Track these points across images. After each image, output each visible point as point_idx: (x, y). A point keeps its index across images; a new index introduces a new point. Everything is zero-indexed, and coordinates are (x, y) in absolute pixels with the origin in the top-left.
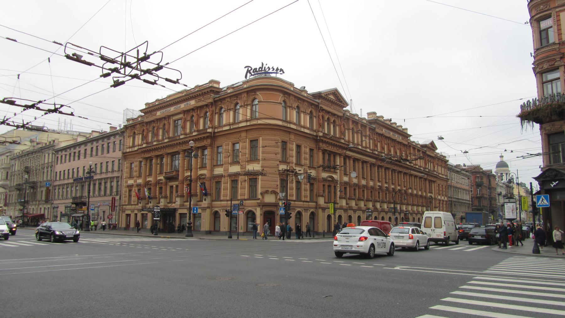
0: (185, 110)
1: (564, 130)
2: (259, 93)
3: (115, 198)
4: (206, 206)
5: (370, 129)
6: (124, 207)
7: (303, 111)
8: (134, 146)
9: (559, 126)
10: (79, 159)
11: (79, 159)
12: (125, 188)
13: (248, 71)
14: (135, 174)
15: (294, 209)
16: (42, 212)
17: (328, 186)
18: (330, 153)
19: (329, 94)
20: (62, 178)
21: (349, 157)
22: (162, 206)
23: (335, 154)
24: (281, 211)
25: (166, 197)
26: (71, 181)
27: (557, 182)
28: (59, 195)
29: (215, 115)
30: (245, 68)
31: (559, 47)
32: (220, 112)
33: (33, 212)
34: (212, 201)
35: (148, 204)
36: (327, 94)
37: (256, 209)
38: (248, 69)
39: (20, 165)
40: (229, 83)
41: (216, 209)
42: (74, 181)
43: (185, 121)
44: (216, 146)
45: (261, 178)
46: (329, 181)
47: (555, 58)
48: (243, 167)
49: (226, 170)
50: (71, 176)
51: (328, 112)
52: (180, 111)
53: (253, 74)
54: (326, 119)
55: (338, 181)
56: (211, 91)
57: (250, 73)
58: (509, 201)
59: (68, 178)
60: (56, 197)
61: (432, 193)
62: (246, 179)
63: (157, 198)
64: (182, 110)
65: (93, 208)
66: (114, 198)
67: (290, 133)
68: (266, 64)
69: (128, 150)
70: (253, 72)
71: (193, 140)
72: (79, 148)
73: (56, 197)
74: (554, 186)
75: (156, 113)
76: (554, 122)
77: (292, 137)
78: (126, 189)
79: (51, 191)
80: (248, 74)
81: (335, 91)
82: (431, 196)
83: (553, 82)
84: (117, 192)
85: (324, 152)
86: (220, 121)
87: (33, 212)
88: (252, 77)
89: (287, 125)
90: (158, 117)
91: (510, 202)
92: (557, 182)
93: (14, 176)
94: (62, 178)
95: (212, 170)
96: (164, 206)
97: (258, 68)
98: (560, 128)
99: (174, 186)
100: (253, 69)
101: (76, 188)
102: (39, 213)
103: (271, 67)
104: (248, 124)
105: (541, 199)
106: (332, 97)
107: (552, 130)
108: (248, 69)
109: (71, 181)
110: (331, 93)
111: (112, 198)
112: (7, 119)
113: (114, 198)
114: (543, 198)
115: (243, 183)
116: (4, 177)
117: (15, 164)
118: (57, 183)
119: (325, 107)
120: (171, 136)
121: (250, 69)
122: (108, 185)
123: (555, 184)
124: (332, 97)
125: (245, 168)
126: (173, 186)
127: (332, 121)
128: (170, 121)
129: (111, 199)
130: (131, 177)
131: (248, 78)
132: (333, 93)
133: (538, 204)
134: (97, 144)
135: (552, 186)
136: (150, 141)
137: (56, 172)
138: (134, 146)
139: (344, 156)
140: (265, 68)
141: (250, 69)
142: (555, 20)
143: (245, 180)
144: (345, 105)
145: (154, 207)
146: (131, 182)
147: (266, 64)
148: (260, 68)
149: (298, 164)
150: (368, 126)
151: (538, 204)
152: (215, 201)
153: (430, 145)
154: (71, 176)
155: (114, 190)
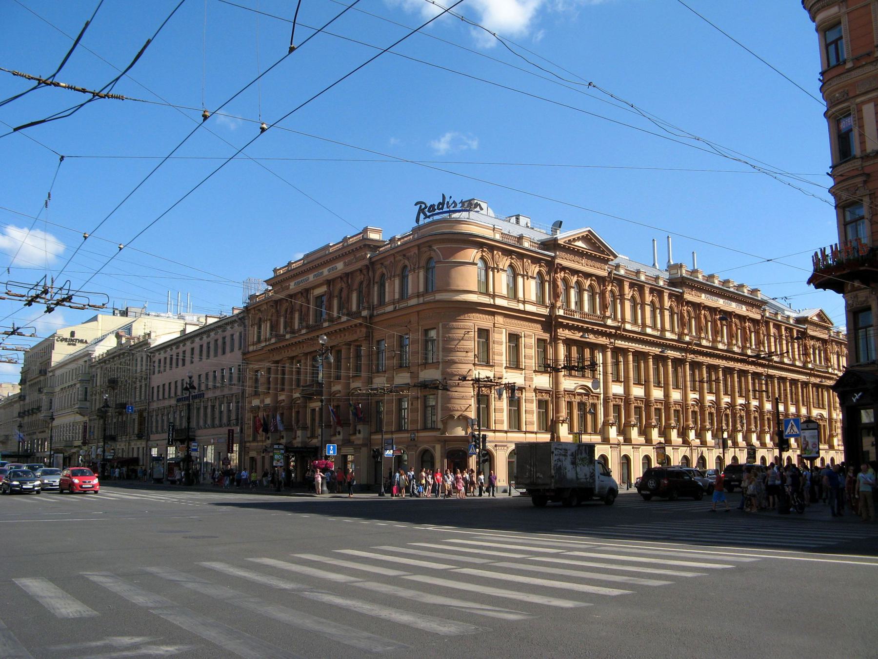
0: (330, 279)
1: (870, 305)
2: (437, 248)
3: (233, 430)
4: (360, 442)
5: (671, 296)
6: (248, 444)
7: (522, 273)
8: (259, 341)
9: (864, 299)
10: (184, 365)
11: (184, 365)
12: (248, 412)
13: (421, 210)
14: (261, 389)
15: (506, 446)
16: (135, 455)
17: (578, 403)
18: (581, 345)
19: (574, 239)
20: (161, 397)
21: (624, 351)
22: (299, 442)
23: (593, 347)
24: (471, 449)
25: (305, 428)
26: (173, 402)
27: (860, 394)
28: (157, 427)
29: (374, 287)
30: (416, 205)
31: (862, 165)
32: (402, 273)
33: (123, 455)
34: (371, 433)
35: (355, 434)
36: (569, 240)
37: (434, 447)
38: (421, 206)
39: (102, 376)
40: (93, 338)
41: (426, 446)
42: (177, 401)
43: (330, 298)
44: (375, 341)
45: (442, 394)
46: (580, 394)
47: (855, 183)
48: (414, 375)
49: (390, 380)
50: (173, 394)
51: (574, 272)
52: (322, 282)
53: (428, 214)
54: (573, 284)
55: (600, 394)
56: (365, 245)
57: (425, 214)
58: (807, 426)
59: (170, 397)
60: (154, 429)
61: (823, 408)
62: (419, 396)
63: (331, 426)
64: (324, 279)
65: (196, 448)
66: (231, 431)
67: (493, 314)
68: (451, 197)
69: (251, 348)
70: (429, 211)
71: (325, 334)
72: (183, 346)
73: (154, 429)
74: (857, 400)
75: (289, 285)
76: (857, 292)
77: (499, 319)
78: (250, 414)
79: (147, 418)
80: (422, 216)
81: (587, 233)
82: (821, 415)
83: (858, 222)
84: (237, 419)
85: (569, 343)
86: (382, 294)
87: (123, 455)
88: (427, 220)
89: (488, 300)
90: (292, 292)
91: (810, 428)
92: (860, 394)
93: (95, 395)
94: (161, 397)
95: (370, 381)
96: (302, 442)
97: (436, 204)
98: (864, 301)
99: (317, 409)
100: (428, 205)
101: (181, 413)
102: (131, 456)
103: (458, 202)
104: (421, 300)
105: (790, 425)
106: (580, 244)
107: (855, 305)
108: (421, 206)
109: (173, 402)
110: (578, 238)
111: (229, 430)
112: (18, 328)
113: (231, 431)
114: (793, 424)
115: (415, 403)
116: (81, 397)
117: (97, 375)
118: (154, 406)
119: (565, 263)
120: (311, 323)
121: (423, 206)
122: (224, 408)
123: (857, 397)
124: (580, 244)
125: (418, 377)
126: (315, 409)
127: (587, 288)
128: (309, 297)
129: (227, 432)
130: (256, 394)
131: (421, 222)
132: (583, 236)
133: (786, 433)
134: (177, 351)
135: (854, 400)
136: (296, 327)
137: (153, 388)
138: (259, 341)
139: (611, 348)
140: (448, 202)
141: (423, 206)
142: (855, 117)
143: (418, 398)
144: (610, 256)
145: (272, 445)
146: (256, 402)
147: (451, 197)
148: (440, 203)
149: (515, 364)
150: (665, 291)
151: (786, 433)
152: (376, 432)
153: (815, 318)
154: (173, 394)
155: (233, 417)
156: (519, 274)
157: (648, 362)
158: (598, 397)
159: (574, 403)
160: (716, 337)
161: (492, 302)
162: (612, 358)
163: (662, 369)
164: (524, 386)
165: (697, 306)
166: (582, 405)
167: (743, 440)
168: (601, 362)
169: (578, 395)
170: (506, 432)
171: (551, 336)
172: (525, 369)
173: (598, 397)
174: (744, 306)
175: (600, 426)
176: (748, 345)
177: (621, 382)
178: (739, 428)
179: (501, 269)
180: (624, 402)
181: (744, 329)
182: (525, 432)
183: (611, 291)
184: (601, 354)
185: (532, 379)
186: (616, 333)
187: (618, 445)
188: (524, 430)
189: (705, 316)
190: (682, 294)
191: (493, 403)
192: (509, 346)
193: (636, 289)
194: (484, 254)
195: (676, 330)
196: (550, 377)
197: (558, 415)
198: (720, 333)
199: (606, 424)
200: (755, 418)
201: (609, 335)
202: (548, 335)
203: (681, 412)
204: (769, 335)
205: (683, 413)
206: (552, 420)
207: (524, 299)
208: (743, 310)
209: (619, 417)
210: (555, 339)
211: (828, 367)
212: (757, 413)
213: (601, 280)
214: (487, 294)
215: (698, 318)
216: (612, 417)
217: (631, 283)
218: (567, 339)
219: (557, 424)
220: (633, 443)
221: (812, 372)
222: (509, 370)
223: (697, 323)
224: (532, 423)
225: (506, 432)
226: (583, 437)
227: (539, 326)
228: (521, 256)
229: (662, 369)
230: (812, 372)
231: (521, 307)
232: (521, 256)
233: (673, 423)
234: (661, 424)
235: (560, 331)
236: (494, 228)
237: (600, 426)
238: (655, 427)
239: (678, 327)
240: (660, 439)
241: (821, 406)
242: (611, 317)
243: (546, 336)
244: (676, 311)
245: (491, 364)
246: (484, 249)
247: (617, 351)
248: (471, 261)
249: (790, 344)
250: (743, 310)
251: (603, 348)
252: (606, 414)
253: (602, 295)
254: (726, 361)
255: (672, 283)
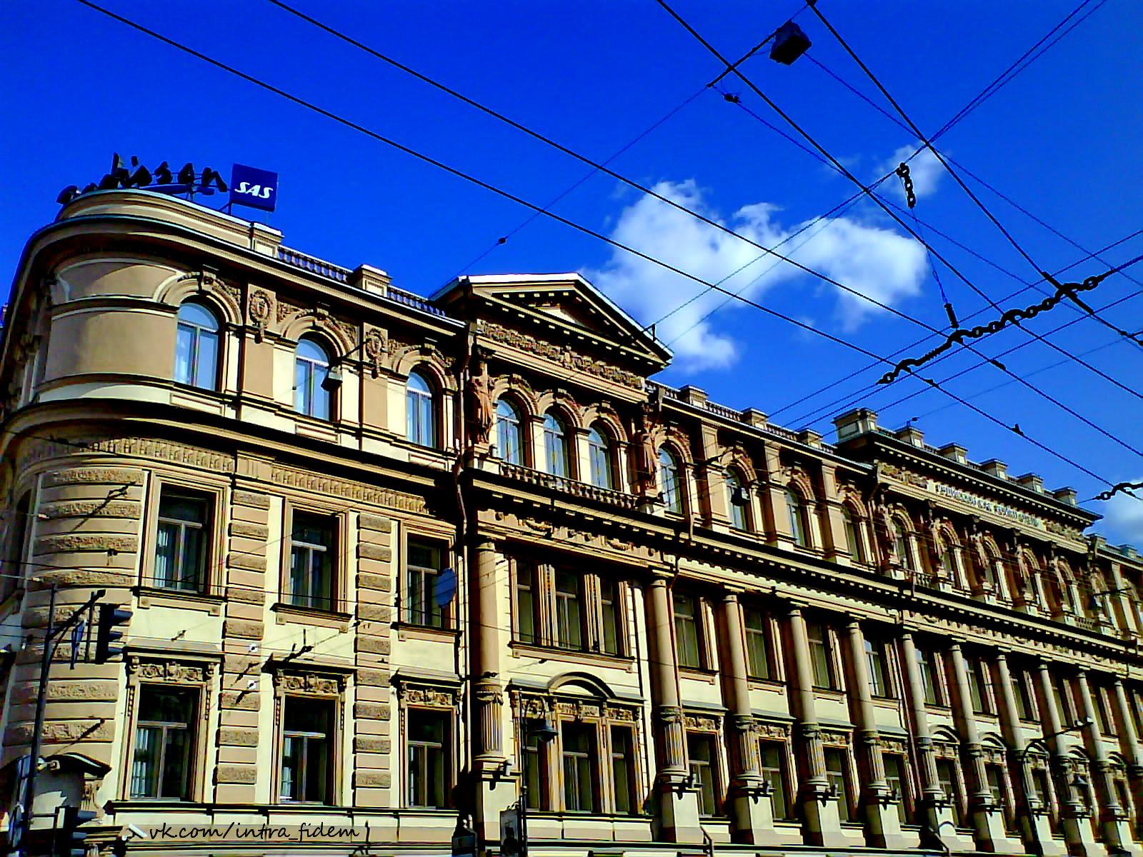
5: (842, 476)
61: (619, 654)
82: (600, 693)
150: (824, 461)
156: (445, 391)
157: (952, 657)
158: (634, 709)
159: (599, 730)
160: (980, 582)
161: (230, 414)
162: (1012, 675)
163: (1030, 682)
164: (350, 664)
165: (918, 508)
166: (579, 735)
167: (1098, 841)
168: (990, 682)
169: (560, 700)
170: (264, 811)
171: (459, 530)
172: (225, 599)
173: (634, 709)
174: (1039, 520)
175: (644, 793)
176: (1066, 607)
177: (713, 673)
178: (1119, 811)
179: (384, 370)
180: (793, 735)
181: (1048, 574)
182: (210, 809)
183: (667, 446)
184: (638, 592)
185: (383, 649)
186: (677, 538)
187: (704, 848)
188: (348, 803)
189: (942, 533)
190: (873, 472)
191: (214, 713)
192: (747, 633)
193: (851, 486)
194: (795, 477)
195: (449, 442)
196: (457, 645)
197: (667, 771)
198: (1028, 583)
199: (663, 787)
200: (1118, 784)
201: (657, 543)
202: (451, 528)
203: (906, 761)
204: (1114, 592)
205: (912, 762)
206: (917, 800)
207: (361, 424)
208: (1039, 528)
209: (1002, 792)
210: (471, 541)
211: (644, 500)
212: (1119, 772)
213: (627, 411)
214: (216, 393)
215: (924, 535)
216: (884, 783)
217: (782, 451)
218: (748, 593)
219: (666, 796)
220: (679, 841)
221: (1132, 651)
222: (406, 633)
223: (634, 458)
224: (381, 784)
225: (396, 814)
226: (531, 823)
227: (419, 502)
228: (354, 316)
229: (1030, 682)
230: (1132, 651)
231: (348, 442)
232: (354, 316)
233: (989, 798)
234: (1007, 802)
235: (486, 517)
236: (252, 230)
237: (644, 793)
238: (992, 809)
239: (457, 434)
240: (846, 833)
241: (437, 622)
242: (902, 567)
243: (445, 530)
244: (864, 514)
245: (213, 591)
246: (796, 468)
247: (687, 590)
248: (154, 300)
249: (690, 471)
250: (1039, 528)
251: (644, 579)
252: (663, 760)
253: (636, 449)
254: (922, 614)
255: (844, 449)
